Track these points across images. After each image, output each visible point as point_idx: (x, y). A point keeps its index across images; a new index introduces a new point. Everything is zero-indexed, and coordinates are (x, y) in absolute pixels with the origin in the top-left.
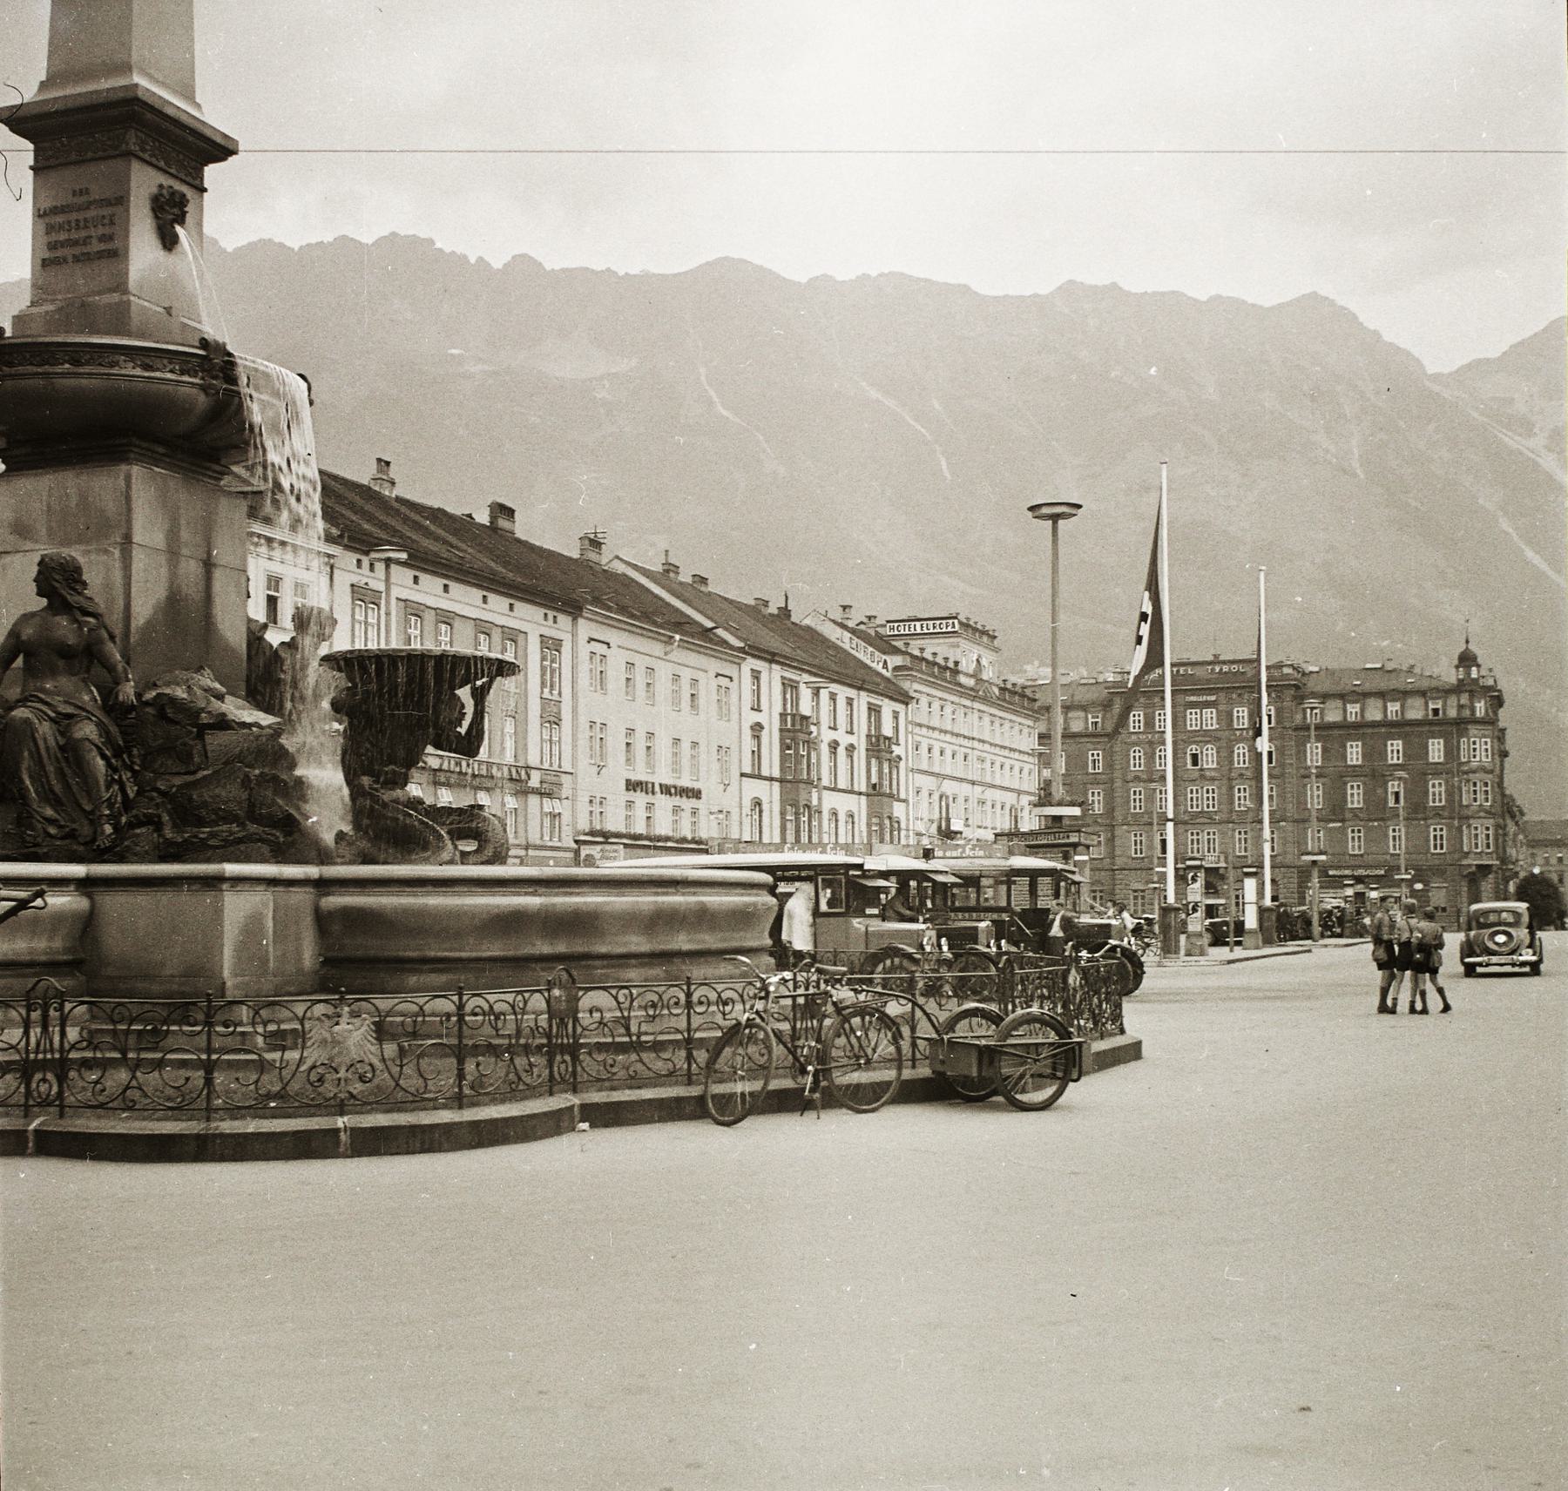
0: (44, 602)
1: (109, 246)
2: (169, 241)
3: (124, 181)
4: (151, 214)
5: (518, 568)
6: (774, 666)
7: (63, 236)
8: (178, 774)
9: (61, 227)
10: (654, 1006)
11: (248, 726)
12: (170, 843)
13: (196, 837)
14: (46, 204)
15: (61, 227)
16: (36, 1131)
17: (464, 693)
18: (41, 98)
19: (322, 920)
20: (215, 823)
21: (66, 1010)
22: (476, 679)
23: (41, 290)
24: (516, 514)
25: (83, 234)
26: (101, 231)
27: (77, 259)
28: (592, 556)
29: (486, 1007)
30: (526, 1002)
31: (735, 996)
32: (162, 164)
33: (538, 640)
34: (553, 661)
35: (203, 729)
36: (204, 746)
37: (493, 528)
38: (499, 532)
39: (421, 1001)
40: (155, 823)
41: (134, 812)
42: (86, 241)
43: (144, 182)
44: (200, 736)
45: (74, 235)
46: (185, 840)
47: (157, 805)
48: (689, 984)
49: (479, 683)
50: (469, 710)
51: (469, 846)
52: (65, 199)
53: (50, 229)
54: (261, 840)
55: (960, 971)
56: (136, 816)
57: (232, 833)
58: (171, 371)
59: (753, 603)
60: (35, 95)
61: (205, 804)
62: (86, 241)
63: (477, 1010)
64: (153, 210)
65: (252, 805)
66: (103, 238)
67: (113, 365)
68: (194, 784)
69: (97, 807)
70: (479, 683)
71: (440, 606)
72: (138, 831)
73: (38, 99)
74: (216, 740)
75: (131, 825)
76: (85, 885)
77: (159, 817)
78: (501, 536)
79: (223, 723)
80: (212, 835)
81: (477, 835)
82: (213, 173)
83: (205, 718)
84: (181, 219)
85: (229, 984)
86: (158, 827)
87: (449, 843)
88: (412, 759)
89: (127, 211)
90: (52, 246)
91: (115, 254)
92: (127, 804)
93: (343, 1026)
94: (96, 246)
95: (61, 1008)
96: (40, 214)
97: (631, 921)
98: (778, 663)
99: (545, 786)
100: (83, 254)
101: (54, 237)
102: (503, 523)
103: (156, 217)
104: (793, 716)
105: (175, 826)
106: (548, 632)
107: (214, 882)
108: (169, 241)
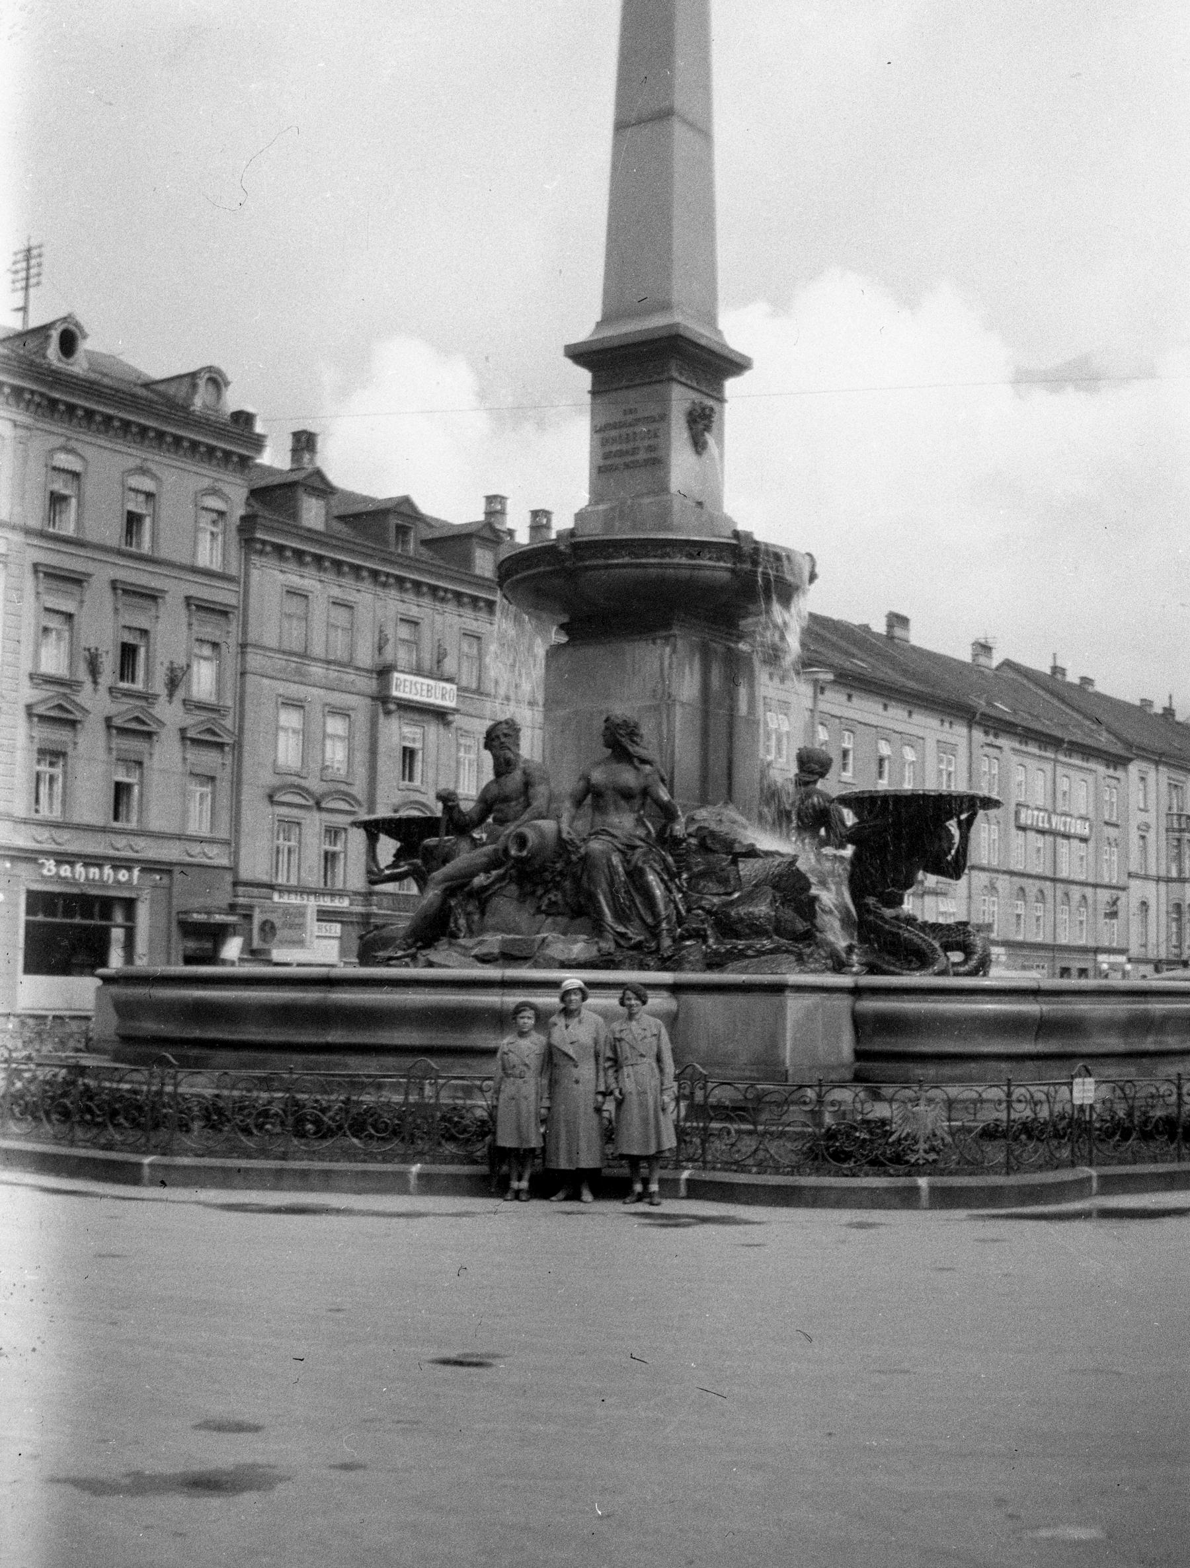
0: (610, 751)
1: (653, 455)
2: (699, 445)
3: (665, 401)
4: (686, 425)
5: (913, 676)
6: (1161, 768)
7: (615, 448)
8: (718, 894)
9: (614, 440)
10: (1152, 1097)
11: (768, 854)
12: (716, 953)
13: (735, 948)
14: (602, 421)
15: (614, 440)
16: (688, 1180)
17: (952, 826)
18: (600, 336)
19: (858, 1021)
20: (747, 937)
21: (709, 1089)
22: (961, 813)
23: (597, 495)
24: (912, 624)
25: (630, 446)
26: (646, 443)
27: (627, 466)
28: (982, 660)
29: (1028, 1096)
30: (1056, 1092)
31: (1043, 1097)
32: (695, 385)
33: (934, 744)
34: (949, 762)
35: (736, 858)
36: (738, 872)
37: (890, 637)
38: (896, 641)
39: (980, 1089)
40: (701, 936)
41: (686, 926)
42: (635, 451)
43: (680, 398)
44: (734, 862)
45: (624, 447)
46: (728, 951)
47: (703, 922)
48: (1009, 1085)
49: (963, 817)
50: (957, 840)
51: (956, 957)
52: (618, 417)
53: (604, 442)
54: (787, 951)
55: (173, 1056)
56: (687, 930)
57: (764, 946)
58: (710, 559)
59: (1138, 703)
60: (592, 335)
61: (741, 920)
62: (635, 451)
63: (1022, 1098)
64: (688, 422)
65: (778, 920)
66: (651, 449)
67: (667, 555)
68: (732, 903)
69: (659, 924)
70: (963, 817)
71: (846, 715)
72: (688, 943)
73: (596, 337)
74: (747, 868)
75: (683, 938)
76: (675, 989)
77: (705, 930)
78: (897, 645)
79: (752, 853)
80: (749, 947)
81: (966, 948)
82: (732, 386)
83: (737, 848)
84: (707, 428)
85: (790, 1072)
86: (705, 939)
87: (942, 954)
88: (909, 883)
89: (669, 424)
90: (606, 456)
91: (657, 462)
92: (680, 921)
93: (921, 1108)
94: (642, 456)
95: (704, 1088)
96: (597, 430)
97: (1109, 1025)
98: (1166, 764)
99: (940, 885)
100: (632, 462)
101: (607, 449)
102: (898, 632)
103: (691, 429)
104: (1180, 816)
105: (717, 939)
106: (942, 737)
107: (778, 989)
108: (699, 445)
